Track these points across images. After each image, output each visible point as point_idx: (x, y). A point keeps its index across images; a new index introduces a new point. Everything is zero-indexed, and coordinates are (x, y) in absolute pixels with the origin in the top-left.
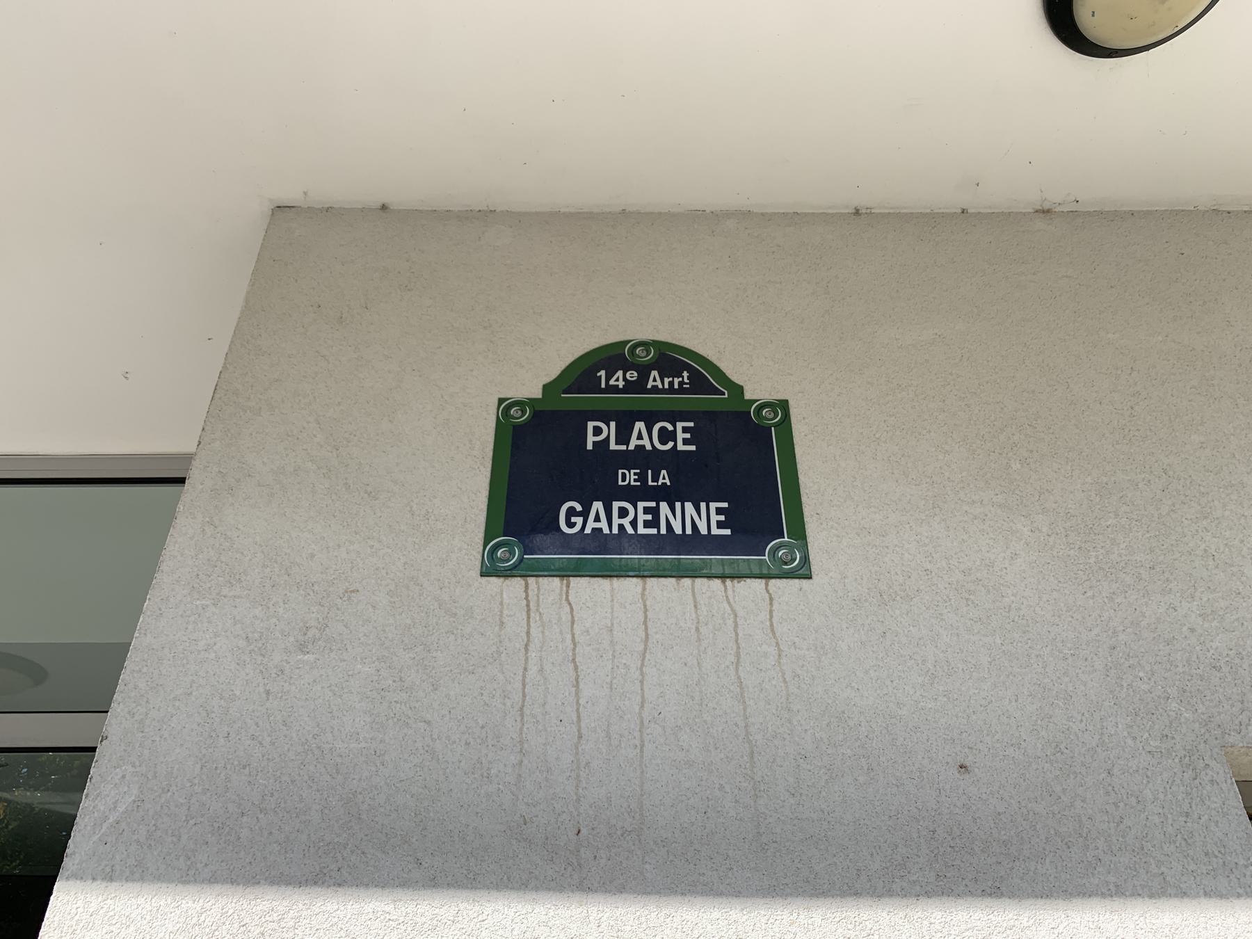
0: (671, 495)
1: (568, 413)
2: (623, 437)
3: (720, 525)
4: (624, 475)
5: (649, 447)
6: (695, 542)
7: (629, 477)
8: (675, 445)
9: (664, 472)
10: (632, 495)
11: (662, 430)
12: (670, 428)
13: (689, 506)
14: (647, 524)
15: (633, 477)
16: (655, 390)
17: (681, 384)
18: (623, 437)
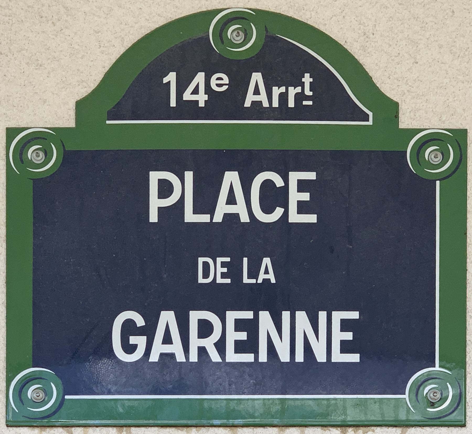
0: (273, 300)
1: (118, 156)
2: (205, 203)
3: (346, 347)
4: (206, 265)
5: (245, 218)
6: (308, 374)
7: (213, 270)
8: (286, 215)
9: (267, 261)
10: (218, 298)
11: (267, 185)
12: (279, 182)
13: (302, 317)
14: (240, 347)
15: (221, 270)
16: (257, 110)
17: (300, 97)
18: (205, 203)
